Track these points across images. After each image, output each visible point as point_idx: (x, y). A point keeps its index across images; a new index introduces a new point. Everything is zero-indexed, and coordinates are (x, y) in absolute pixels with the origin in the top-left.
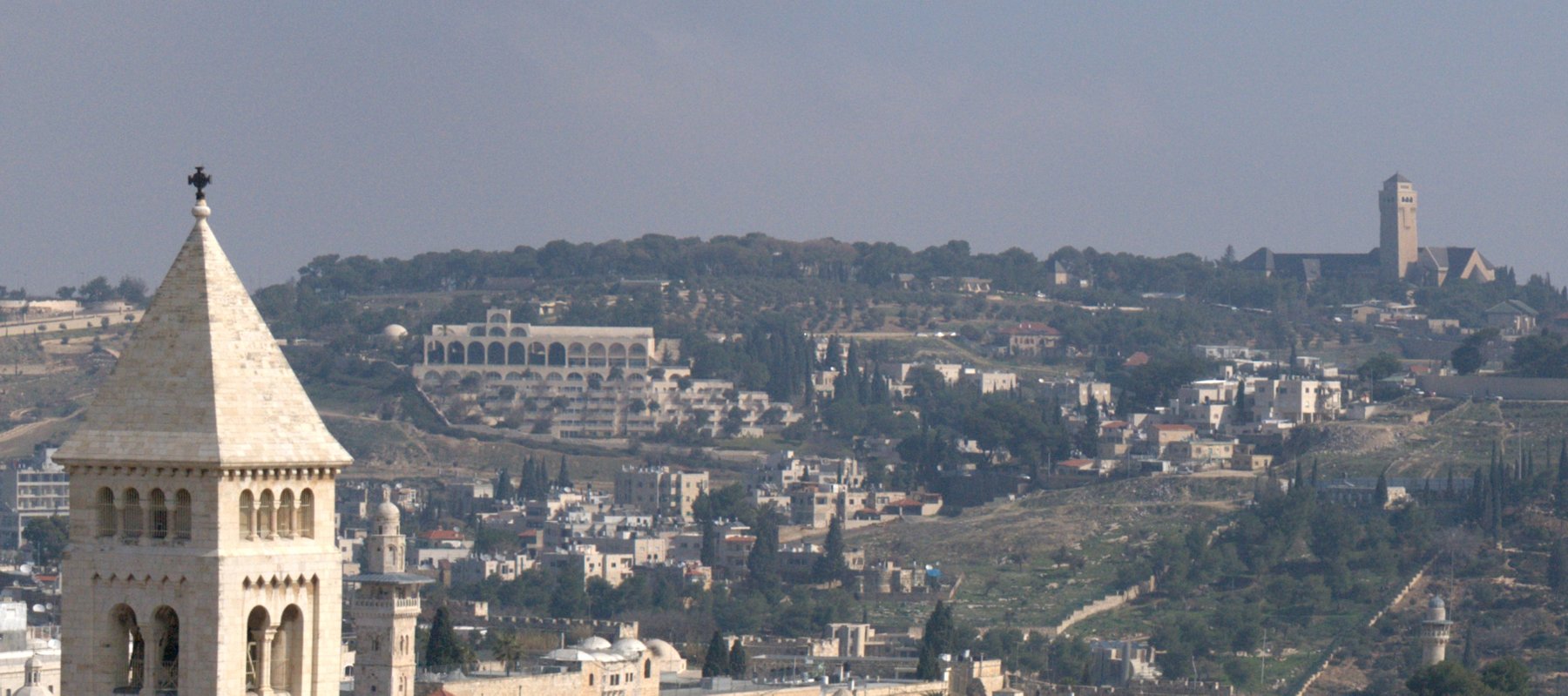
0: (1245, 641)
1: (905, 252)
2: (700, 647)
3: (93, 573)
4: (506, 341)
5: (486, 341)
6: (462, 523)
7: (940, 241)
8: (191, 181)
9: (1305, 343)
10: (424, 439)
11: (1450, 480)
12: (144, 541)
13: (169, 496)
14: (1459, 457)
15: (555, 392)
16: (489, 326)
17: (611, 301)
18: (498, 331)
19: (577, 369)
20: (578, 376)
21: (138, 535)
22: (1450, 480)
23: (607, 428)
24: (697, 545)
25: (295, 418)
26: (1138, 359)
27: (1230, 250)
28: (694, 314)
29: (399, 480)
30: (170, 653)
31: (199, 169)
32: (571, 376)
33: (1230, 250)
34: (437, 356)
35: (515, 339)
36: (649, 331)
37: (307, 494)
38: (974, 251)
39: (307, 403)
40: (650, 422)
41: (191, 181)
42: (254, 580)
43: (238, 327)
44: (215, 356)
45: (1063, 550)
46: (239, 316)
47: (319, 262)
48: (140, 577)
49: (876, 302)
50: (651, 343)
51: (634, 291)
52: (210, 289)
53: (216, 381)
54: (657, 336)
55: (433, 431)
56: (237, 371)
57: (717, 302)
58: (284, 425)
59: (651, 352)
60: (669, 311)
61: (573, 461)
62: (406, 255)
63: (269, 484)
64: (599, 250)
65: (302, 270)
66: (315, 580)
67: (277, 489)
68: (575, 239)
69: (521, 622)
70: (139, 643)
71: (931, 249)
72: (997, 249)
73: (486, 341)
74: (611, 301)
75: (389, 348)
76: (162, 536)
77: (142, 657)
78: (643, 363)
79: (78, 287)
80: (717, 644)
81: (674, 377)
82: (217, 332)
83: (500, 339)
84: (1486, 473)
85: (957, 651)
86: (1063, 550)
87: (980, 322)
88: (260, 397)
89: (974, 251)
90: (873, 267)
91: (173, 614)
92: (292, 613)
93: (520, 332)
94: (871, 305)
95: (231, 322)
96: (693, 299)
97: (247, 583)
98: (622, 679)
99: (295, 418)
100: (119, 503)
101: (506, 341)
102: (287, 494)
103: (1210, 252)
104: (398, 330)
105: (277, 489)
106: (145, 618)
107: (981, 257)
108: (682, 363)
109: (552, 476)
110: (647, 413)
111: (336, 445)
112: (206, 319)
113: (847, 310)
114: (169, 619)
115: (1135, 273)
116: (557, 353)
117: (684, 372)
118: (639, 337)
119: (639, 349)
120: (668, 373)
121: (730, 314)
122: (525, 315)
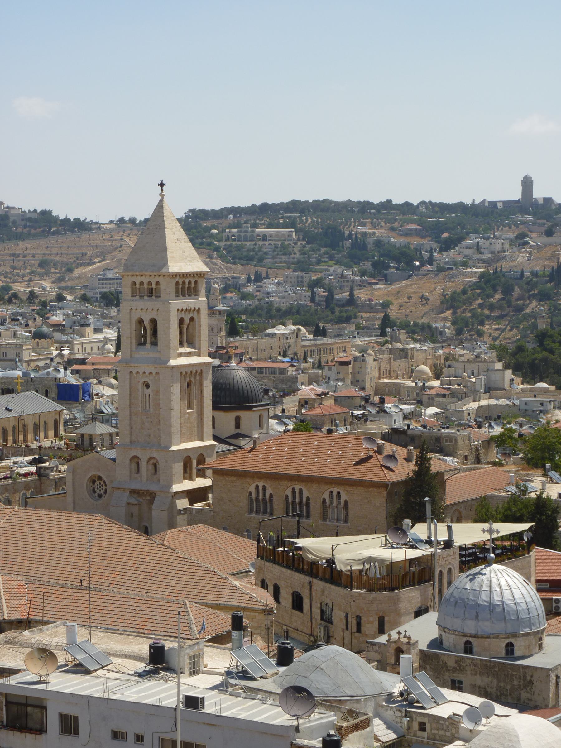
0: (482, 323)
1: (372, 203)
2: (313, 328)
3: (130, 308)
4: (249, 234)
5: (242, 234)
6: (236, 291)
7: (383, 200)
8: (159, 185)
9: (498, 229)
10: (224, 265)
11: (544, 270)
12: (146, 298)
13: (153, 283)
14: (547, 263)
15: (265, 250)
16: (243, 230)
17: (281, 221)
18: (246, 231)
19: (270, 242)
20: (271, 244)
21: (143, 296)
22: (544, 270)
23: (281, 260)
24: (309, 296)
25: (192, 258)
26: (446, 235)
27: (474, 200)
28: (307, 225)
29: (216, 278)
30: (155, 332)
31: (162, 181)
32: (269, 244)
33: (474, 200)
34: (228, 239)
35: (251, 234)
36: (293, 230)
37: (196, 282)
38: (394, 203)
39: (196, 254)
40: (294, 258)
41: (159, 185)
42: (180, 309)
43: (174, 230)
44: (167, 239)
45: (423, 295)
46: (174, 227)
47: (190, 211)
48: (145, 309)
49: (363, 219)
50: (294, 233)
51: (289, 218)
52: (165, 219)
53: (168, 247)
54: (296, 232)
55: (227, 263)
56: (174, 244)
57: (314, 221)
58: (188, 261)
59: (294, 237)
60: (299, 224)
61: (270, 271)
62: (217, 208)
63: (184, 279)
64: (278, 205)
65: (185, 213)
66: (199, 309)
67: (187, 281)
68: (270, 202)
69: (256, 321)
70: (145, 329)
71: (381, 202)
72: (401, 201)
73: (242, 234)
74: (281, 221)
75: (212, 236)
76: (152, 296)
77: (146, 334)
78: (291, 240)
79: (115, 220)
80: (317, 326)
81: (301, 244)
82: (167, 232)
83: (247, 234)
84: (556, 268)
85: (391, 327)
86: (423, 295)
87: (396, 224)
88: (181, 252)
89: (394, 203)
90: (364, 208)
91: (155, 320)
92: (192, 319)
93: (253, 231)
94: (362, 220)
95: (172, 229)
96: (307, 220)
97: (178, 310)
98: (289, 338)
99: (192, 258)
100: (138, 286)
101: (249, 234)
102: (190, 283)
103: (468, 201)
104: (215, 231)
105: (187, 281)
106: (147, 323)
107: (396, 204)
108: (304, 239)
109: (264, 275)
110: (292, 256)
111: (205, 266)
112: (164, 228)
113: (355, 222)
114: (154, 322)
115: (443, 208)
116: (264, 238)
117: (304, 243)
118: (289, 232)
119: (290, 236)
120: (299, 243)
121: (318, 224)
122: (255, 226)
